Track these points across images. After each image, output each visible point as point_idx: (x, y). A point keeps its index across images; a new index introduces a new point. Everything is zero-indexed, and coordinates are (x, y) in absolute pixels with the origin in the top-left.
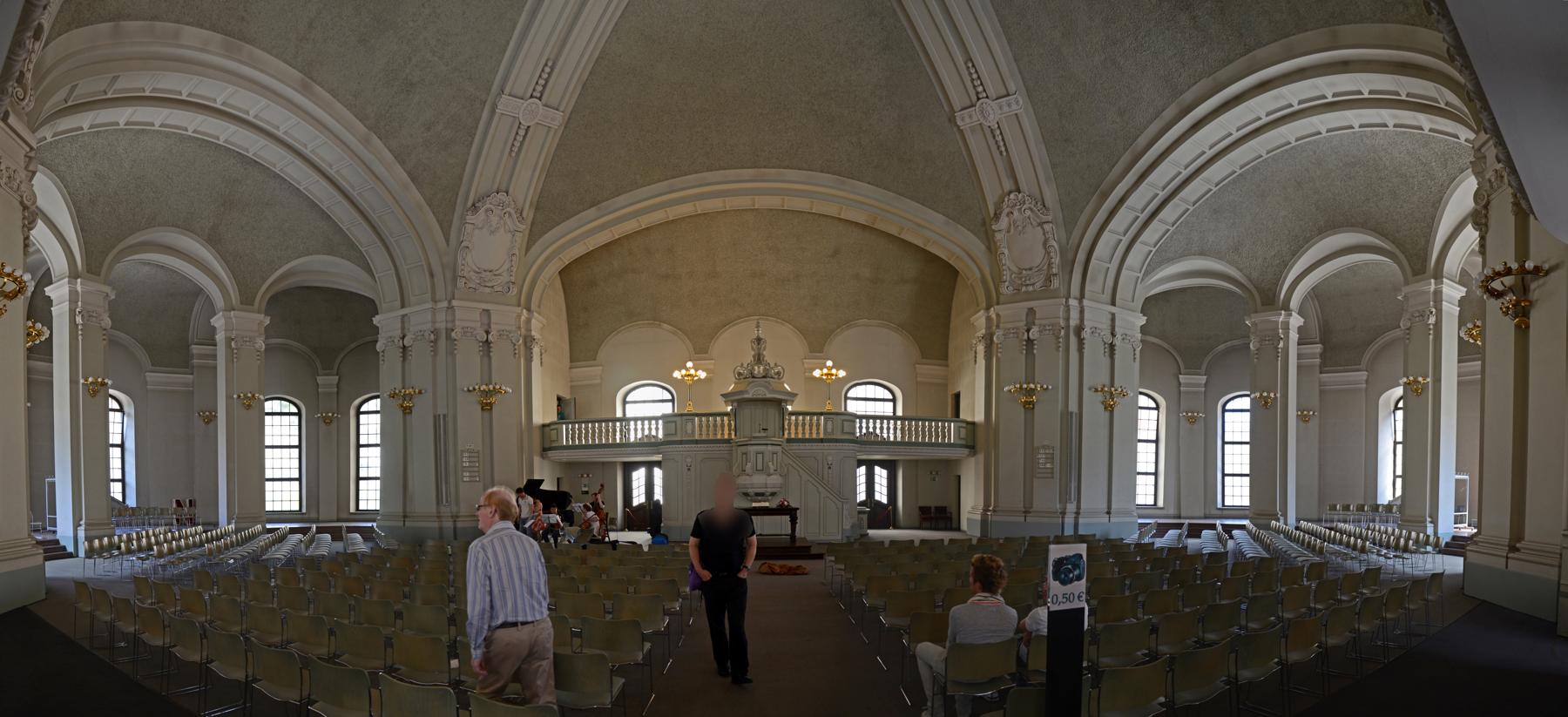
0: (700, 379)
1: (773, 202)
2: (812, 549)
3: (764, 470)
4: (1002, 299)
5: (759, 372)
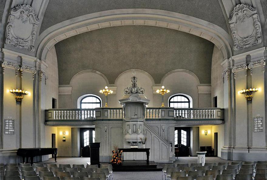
1: (140, 22)
2: (157, 167)
3: (135, 132)
5: (134, 91)
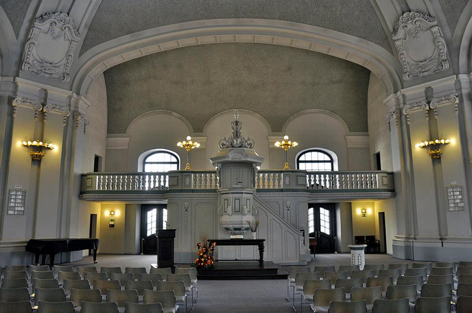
0: (196, 148)
1: (248, 38)
4: (405, 84)
5: (237, 144)
